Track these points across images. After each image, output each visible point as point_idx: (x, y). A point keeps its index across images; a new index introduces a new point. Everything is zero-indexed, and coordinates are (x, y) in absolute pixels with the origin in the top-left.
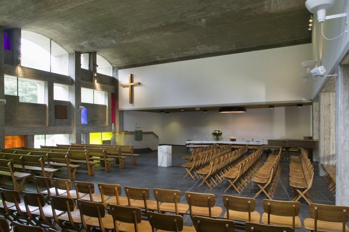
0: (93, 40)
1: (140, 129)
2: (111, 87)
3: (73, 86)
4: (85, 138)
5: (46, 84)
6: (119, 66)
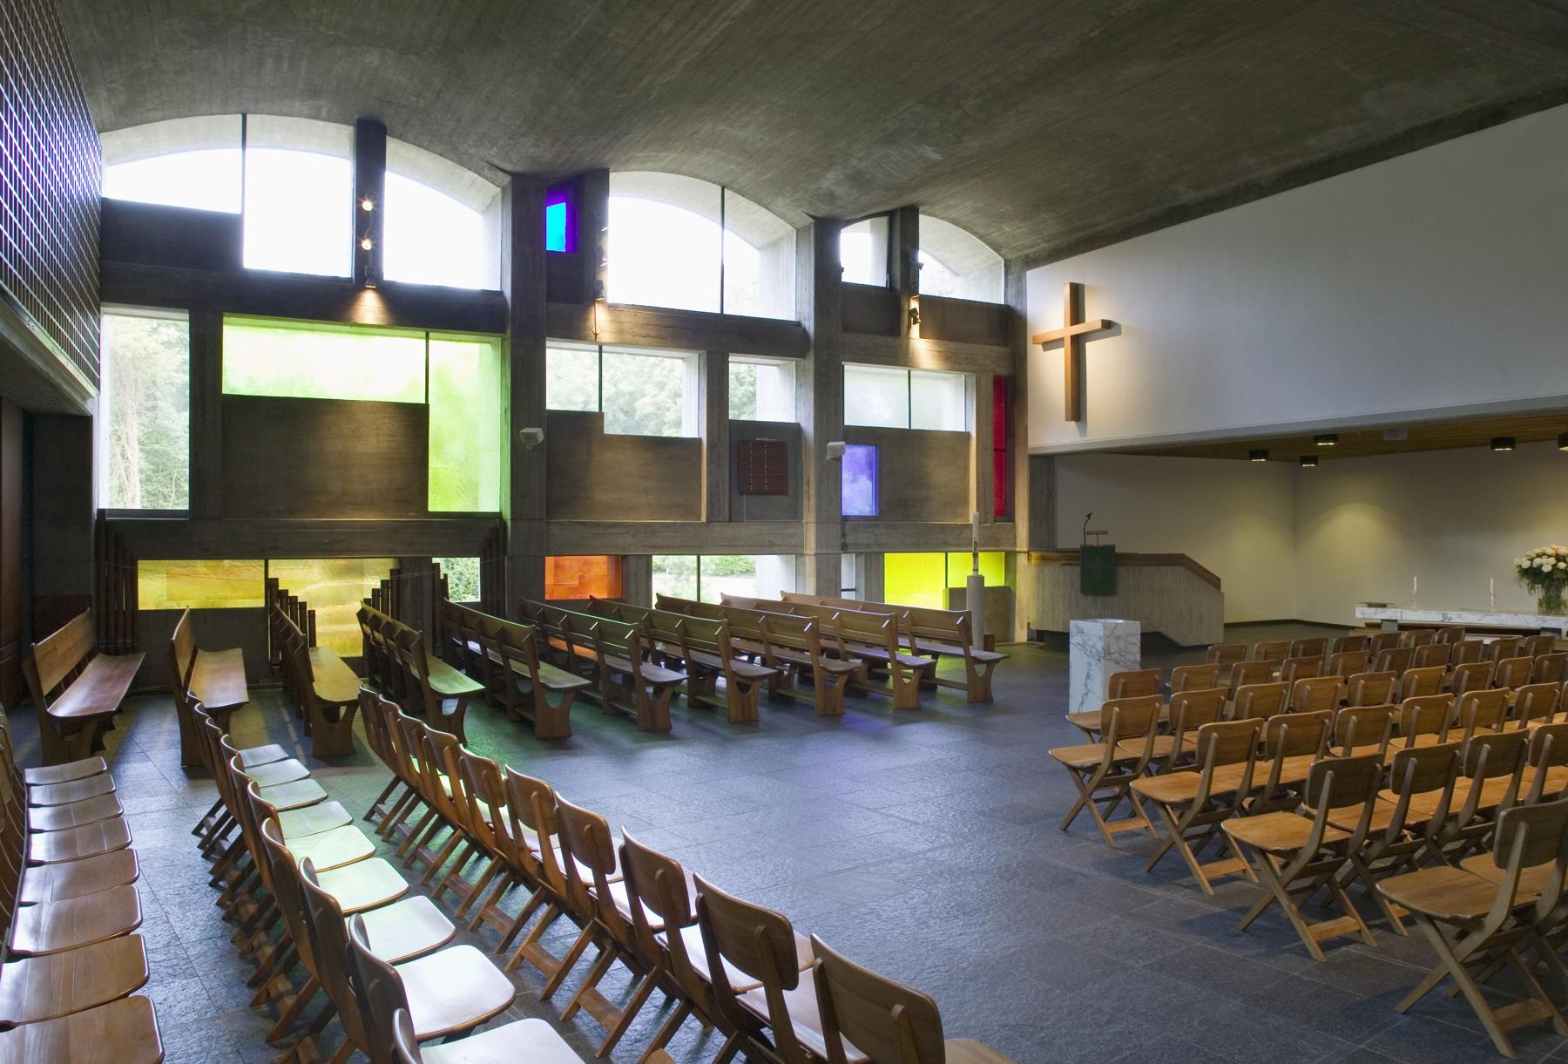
0: (854, 162)
1: (1104, 541)
2: (992, 355)
3: (807, 358)
4: (863, 573)
5: (702, 362)
6: (1026, 252)
